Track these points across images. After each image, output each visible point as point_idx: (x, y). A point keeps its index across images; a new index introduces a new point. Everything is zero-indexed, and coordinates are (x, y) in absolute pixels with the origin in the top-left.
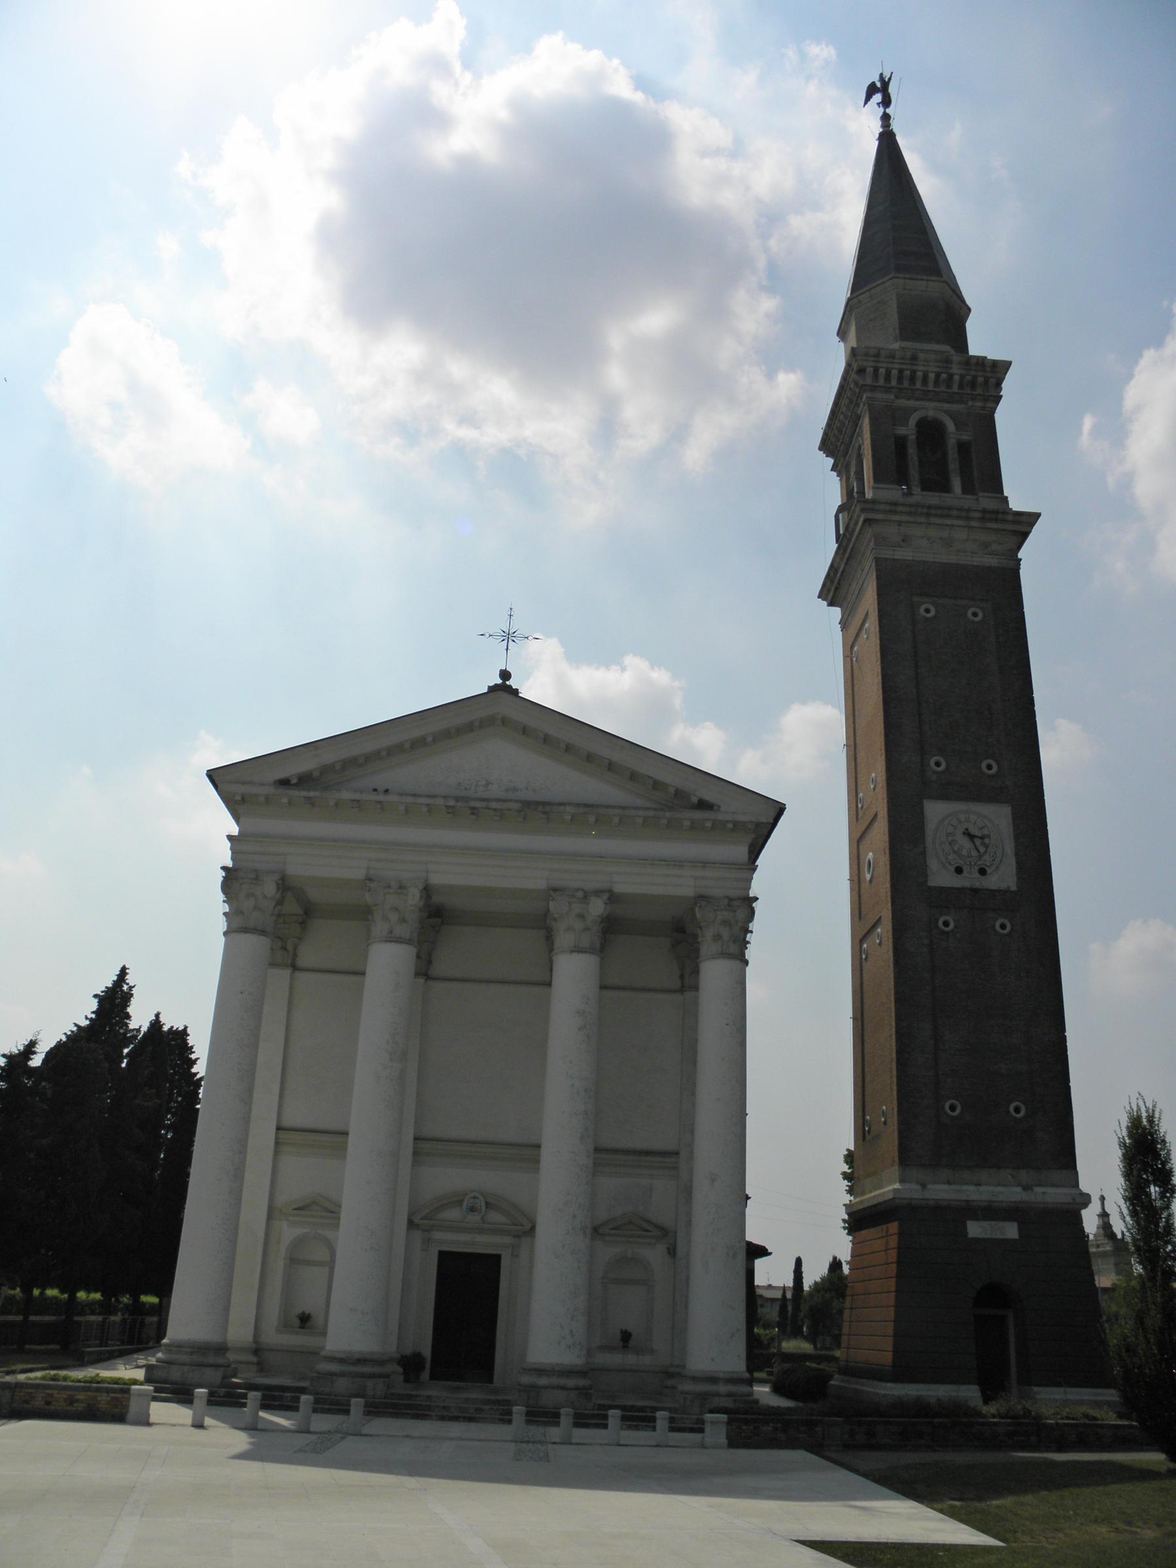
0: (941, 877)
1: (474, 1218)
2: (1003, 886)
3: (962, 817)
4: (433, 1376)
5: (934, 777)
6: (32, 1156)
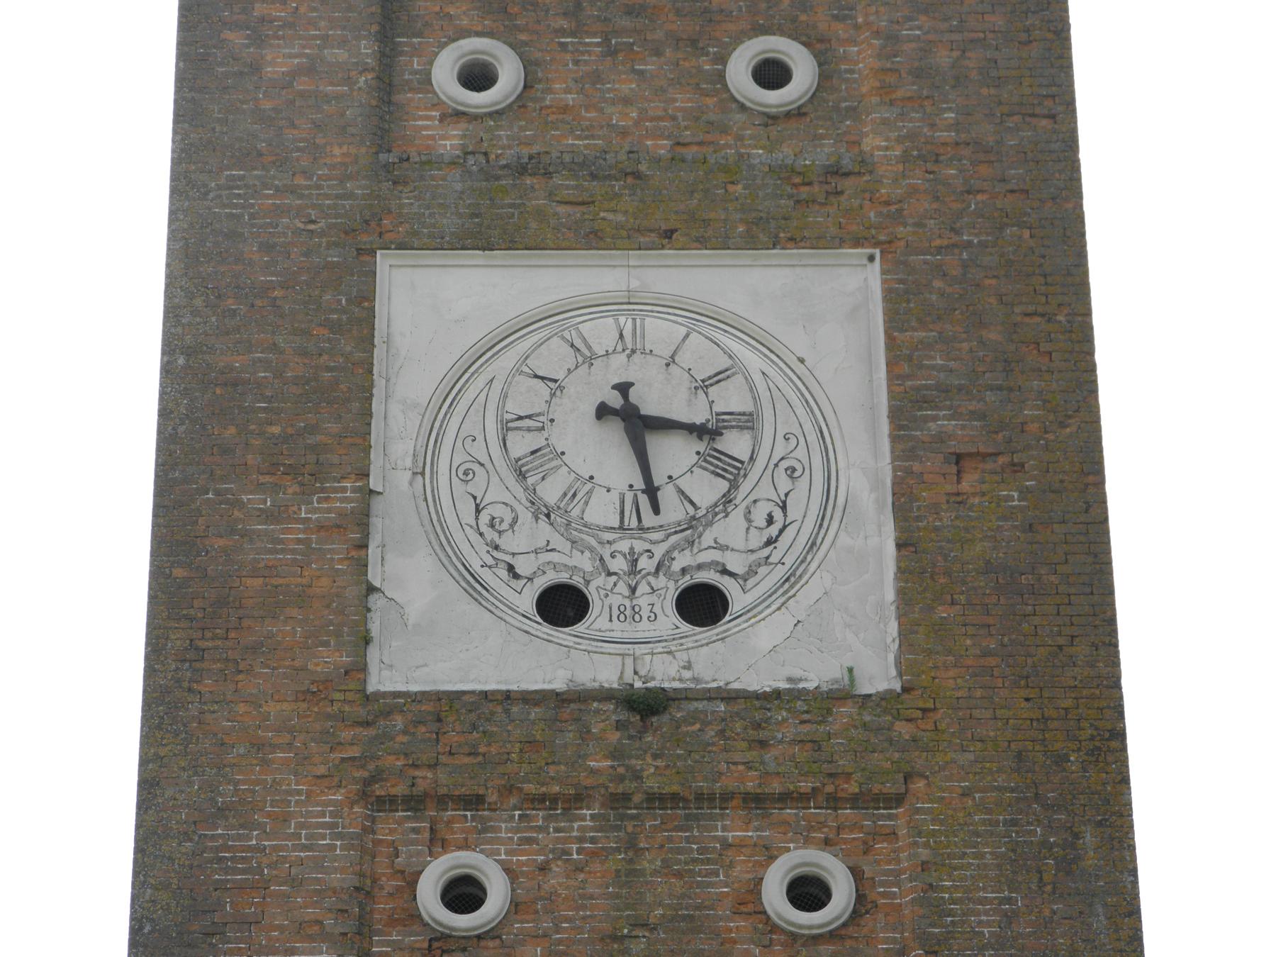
0: (442, 632)
2: (818, 673)
3: (600, 333)
5: (450, 142)
6: (934, 297)
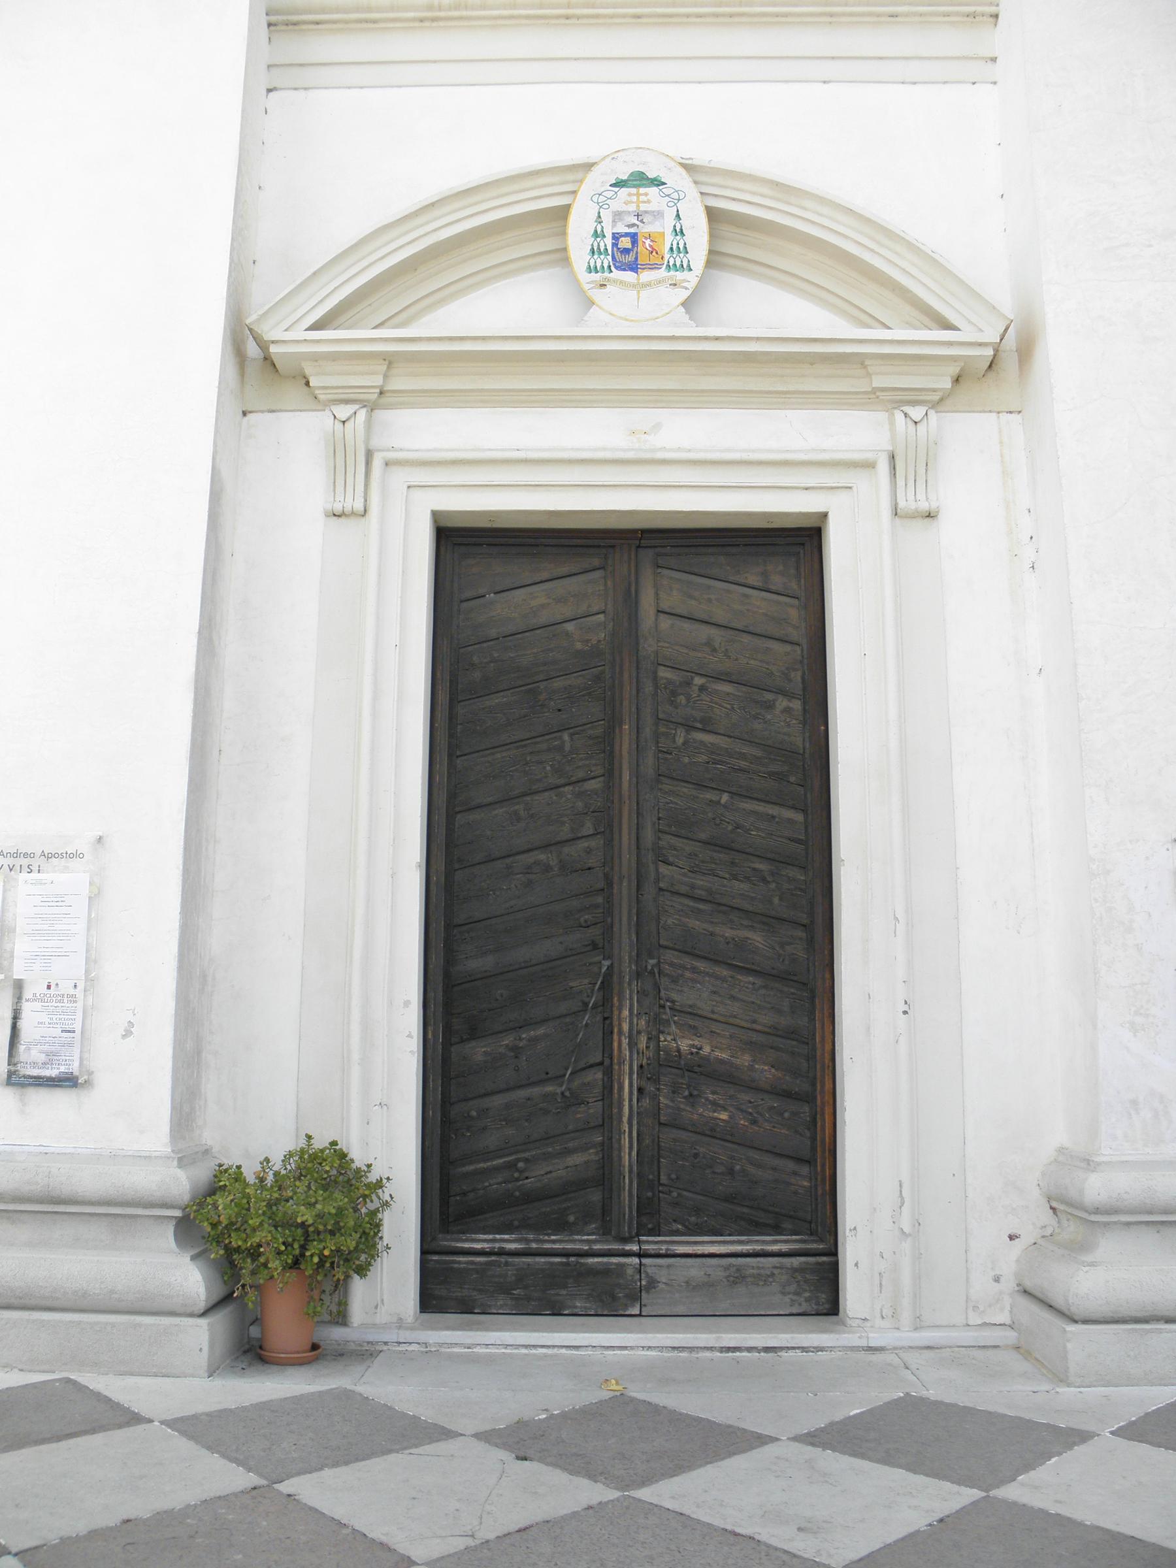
1: (640, 309)
4: (442, 1291)
